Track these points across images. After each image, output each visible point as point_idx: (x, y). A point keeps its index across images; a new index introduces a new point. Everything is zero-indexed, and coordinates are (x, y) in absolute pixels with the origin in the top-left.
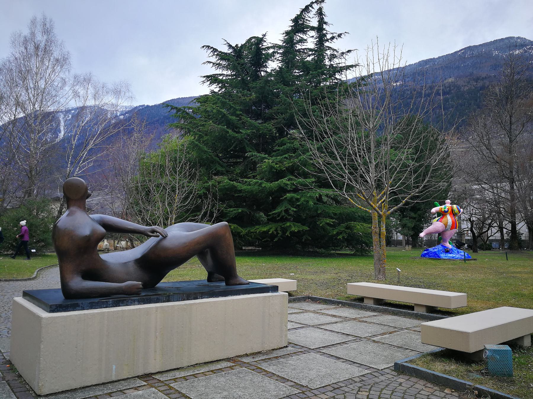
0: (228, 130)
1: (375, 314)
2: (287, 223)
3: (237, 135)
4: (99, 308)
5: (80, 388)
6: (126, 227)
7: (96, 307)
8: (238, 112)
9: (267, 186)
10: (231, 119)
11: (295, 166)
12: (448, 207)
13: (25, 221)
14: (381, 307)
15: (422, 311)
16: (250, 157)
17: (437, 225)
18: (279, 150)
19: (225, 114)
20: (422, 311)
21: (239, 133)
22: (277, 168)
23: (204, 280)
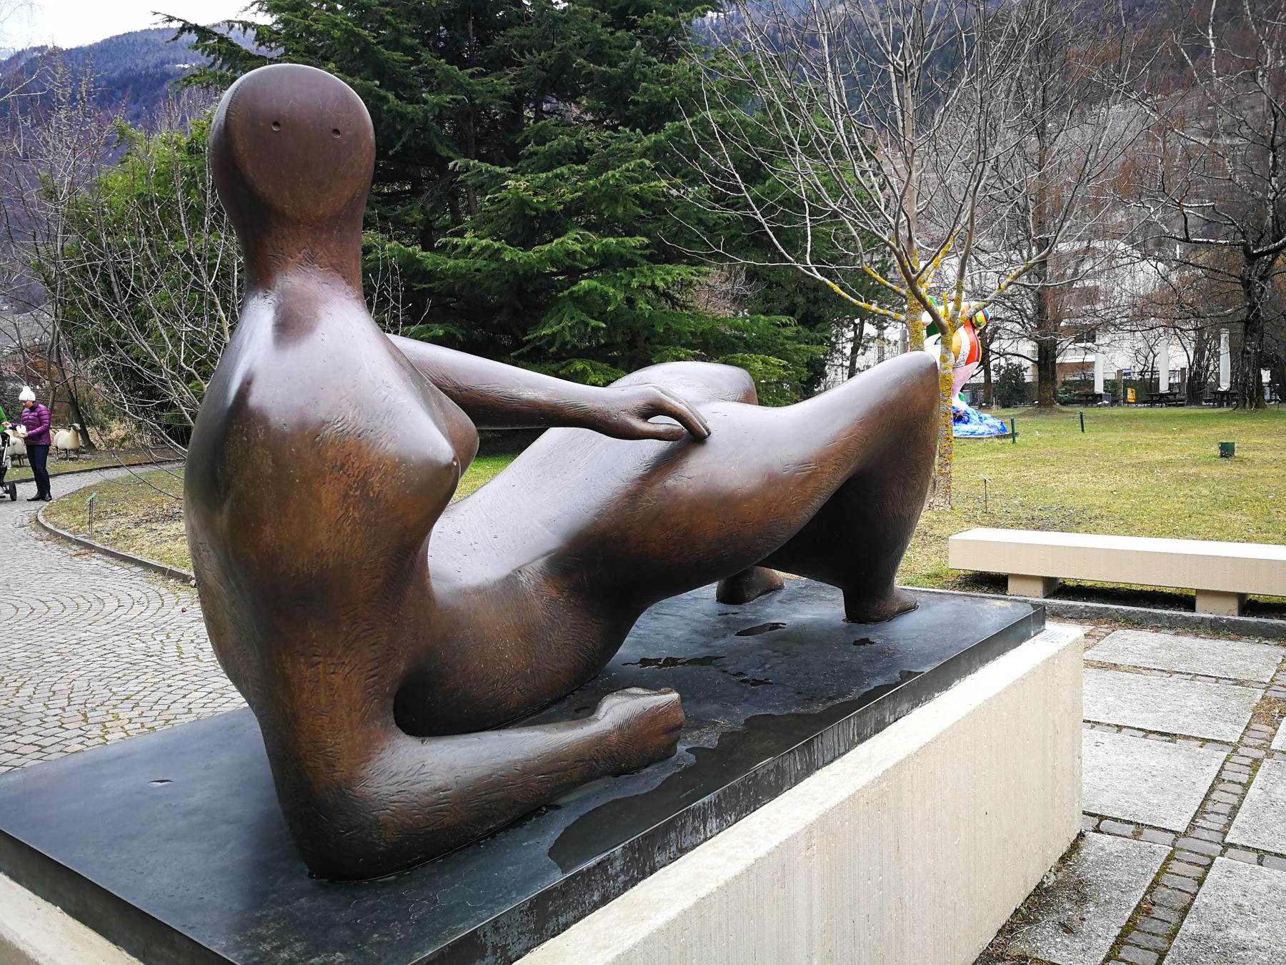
0: (382, 92)
2: (571, 363)
3: (410, 108)
4: (577, 920)
6: (514, 391)
7: (562, 920)
8: (408, 41)
9: (516, 259)
10: (387, 60)
11: (588, 200)
13: (1262, 371)
14: (1078, 603)
15: (1228, 611)
16: (459, 173)
18: (535, 154)
19: (368, 44)
20: (1228, 611)
21: (418, 103)
22: (539, 206)
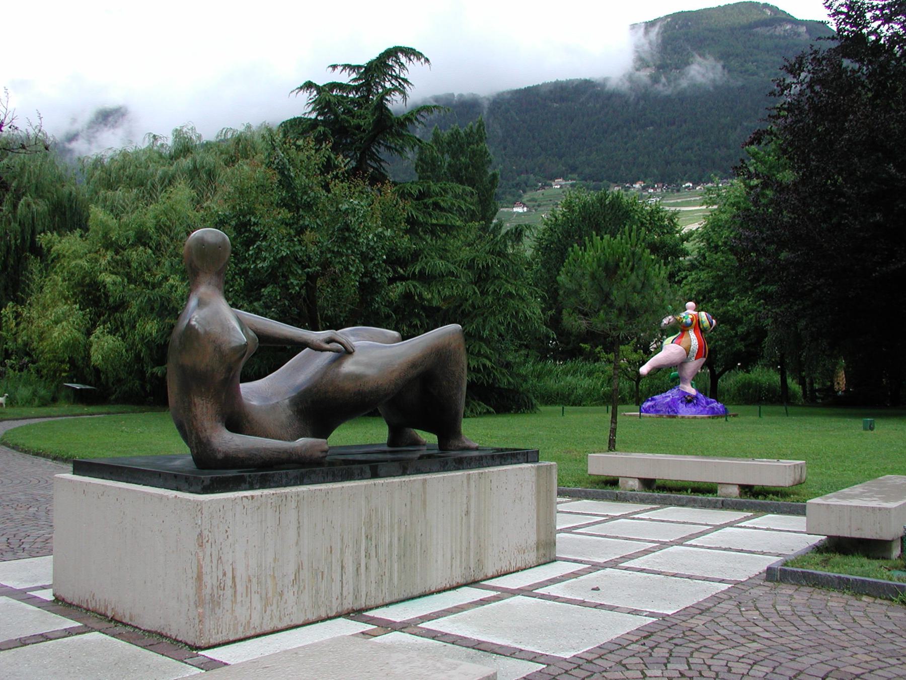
1: (648, 507)
5: (432, 593)
12: (691, 316)
17: (673, 350)
23: (383, 445)
